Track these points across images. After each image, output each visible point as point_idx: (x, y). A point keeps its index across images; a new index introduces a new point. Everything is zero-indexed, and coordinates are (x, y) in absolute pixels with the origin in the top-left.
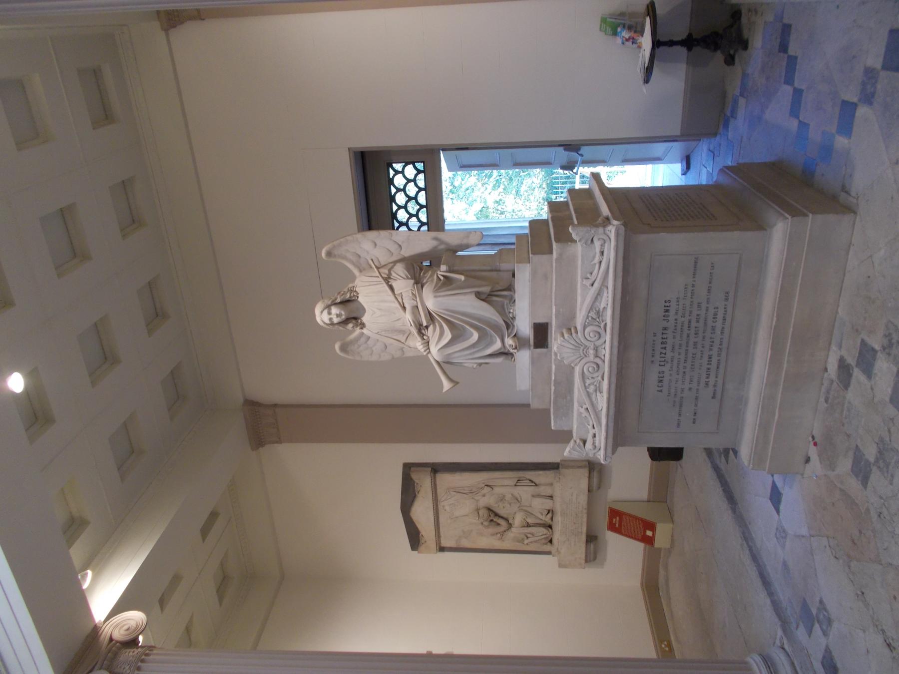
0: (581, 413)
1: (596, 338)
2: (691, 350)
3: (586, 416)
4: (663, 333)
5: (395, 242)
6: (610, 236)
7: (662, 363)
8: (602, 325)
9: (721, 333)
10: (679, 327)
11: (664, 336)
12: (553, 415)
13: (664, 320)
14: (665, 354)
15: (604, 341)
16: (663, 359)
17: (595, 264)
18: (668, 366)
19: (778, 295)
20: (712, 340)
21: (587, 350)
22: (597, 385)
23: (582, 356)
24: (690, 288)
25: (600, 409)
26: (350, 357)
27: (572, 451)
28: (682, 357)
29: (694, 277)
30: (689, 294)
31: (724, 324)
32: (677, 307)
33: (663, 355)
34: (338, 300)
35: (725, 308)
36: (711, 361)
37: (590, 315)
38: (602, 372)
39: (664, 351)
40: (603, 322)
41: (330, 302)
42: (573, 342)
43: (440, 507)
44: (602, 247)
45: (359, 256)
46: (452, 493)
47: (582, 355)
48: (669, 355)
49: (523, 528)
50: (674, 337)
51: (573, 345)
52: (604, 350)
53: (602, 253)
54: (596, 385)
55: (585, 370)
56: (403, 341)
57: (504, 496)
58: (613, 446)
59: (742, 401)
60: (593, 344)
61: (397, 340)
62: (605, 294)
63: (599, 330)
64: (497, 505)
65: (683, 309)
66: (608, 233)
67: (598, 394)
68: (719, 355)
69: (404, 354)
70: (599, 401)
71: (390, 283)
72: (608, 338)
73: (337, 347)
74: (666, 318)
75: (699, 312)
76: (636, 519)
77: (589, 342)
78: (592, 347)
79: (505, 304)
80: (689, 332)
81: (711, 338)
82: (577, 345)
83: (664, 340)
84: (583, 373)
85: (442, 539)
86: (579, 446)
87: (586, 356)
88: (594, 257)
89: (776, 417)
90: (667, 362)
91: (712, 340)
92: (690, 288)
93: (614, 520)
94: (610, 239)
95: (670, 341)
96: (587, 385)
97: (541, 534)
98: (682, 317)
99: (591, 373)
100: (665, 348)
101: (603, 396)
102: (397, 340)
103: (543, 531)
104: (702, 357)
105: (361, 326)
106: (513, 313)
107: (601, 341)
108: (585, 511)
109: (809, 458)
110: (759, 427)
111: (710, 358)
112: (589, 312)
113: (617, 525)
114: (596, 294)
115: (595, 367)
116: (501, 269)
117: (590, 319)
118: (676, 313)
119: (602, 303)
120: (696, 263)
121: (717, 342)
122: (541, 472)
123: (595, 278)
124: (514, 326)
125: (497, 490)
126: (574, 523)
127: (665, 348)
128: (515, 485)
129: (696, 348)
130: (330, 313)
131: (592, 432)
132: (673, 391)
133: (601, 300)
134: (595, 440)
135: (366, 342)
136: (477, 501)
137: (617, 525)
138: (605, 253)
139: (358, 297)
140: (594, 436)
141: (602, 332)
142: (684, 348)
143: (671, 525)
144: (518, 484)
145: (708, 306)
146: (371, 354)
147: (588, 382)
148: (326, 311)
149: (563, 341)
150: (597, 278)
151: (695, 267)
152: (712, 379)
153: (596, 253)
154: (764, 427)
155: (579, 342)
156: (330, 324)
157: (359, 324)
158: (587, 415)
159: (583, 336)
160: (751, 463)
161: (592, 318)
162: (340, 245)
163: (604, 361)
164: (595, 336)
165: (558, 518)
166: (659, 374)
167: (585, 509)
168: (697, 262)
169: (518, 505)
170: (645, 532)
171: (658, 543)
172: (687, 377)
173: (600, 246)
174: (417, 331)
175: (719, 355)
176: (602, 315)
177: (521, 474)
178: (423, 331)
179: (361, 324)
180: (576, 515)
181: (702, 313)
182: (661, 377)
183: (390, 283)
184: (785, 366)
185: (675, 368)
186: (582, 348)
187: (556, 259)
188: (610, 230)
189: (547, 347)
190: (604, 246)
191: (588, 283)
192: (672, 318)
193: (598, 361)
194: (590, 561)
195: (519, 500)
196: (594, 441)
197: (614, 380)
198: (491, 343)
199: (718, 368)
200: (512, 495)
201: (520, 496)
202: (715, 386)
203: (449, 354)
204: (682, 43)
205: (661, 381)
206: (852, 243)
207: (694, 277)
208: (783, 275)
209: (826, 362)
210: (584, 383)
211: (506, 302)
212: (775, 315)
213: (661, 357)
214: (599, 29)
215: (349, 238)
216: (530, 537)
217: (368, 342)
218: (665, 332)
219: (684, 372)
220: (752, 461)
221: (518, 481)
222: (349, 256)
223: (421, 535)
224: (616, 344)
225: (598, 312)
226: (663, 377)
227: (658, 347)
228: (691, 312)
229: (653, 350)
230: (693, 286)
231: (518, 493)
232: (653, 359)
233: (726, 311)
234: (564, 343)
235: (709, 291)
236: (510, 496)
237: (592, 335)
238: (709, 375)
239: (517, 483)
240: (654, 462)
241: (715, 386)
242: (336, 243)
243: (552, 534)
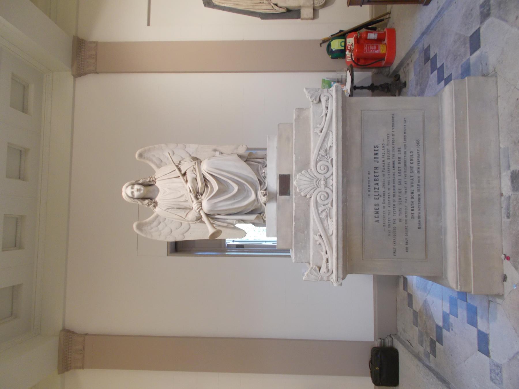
0: (316, 241)
1: (324, 171)
2: (397, 186)
3: (320, 244)
4: (375, 172)
5: (188, 152)
6: (332, 94)
7: (377, 197)
8: (329, 160)
9: (418, 172)
10: (386, 168)
11: (376, 174)
12: (294, 248)
13: (375, 161)
14: (378, 189)
15: (331, 174)
16: (377, 194)
17: (323, 116)
18: (381, 199)
19: (455, 136)
20: (412, 178)
21: (319, 181)
22: (328, 212)
23: (315, 187)
24: (391, 137)
25: (331, 234)
26: (143, 235)
27: (310, 275)
28: (391, 191)
29: (393, 129)
30: (391, 142)
31: (419, 165)
32: (383, 151)
33: (376, 190)
34: (141, 182)
35: (418, 153)
36: (413, 196)
37: (320, 153)
38: (332, 200)
39: (377, 187)
40: (330, 158)
41: (134, 182)
42: (308, 176)
44: (327, 103)
45: (162, 161)
47: (315, 186)
48: (381, 190)
50: (384, 175)
51: (309, 178)
52: (332, 181)
53: (327, 108)
54: (327, 212)
55: (318, 198)
56: (184, 216)
58: (343, 273)
59: (441, 231)
60: (323, 177)
61: (180, 216)
62: (331, 136)
63: (327, 164)
65: (388, 153)
66: (331, 92)
67: (329, 219)
68: (419, 191)
69: (184, 238)
70: (330, 225)
71: (179, 167)
72: (334, 170)
73: (135, 225)
74: (376, 160)
75: (399, 156)
77: (321, 175)
78: (323, 178)
79: (259, 167)
80: (394, 171)
81: (411, 177)
82: (311, 178)
83: (376, 178)
84: (316, 202)
86: (315, 270)
87: (318, 187)
88: (322, 113)
89: (472, 239)
90: (381, 196)
91: (412, 178)
92: (391, 137)
94: (332, 96)
95: (381, 178)
96: (320, 212)
98: (387, 159)
99: (323, 200)
100: (377, 184)
101: (333, 221)
102: (180, 216)
104: (406, 192)
105: (154, 203)
106: (264, 172)
107: (329, 173)
109: (505, 275)
110: (459, 248)
111: (412, 193)
112: (319, 151)
114: (324, 137)
115: (326, 195)
117: (320, 156)
118: (383, 156)
119: (329, 143)
120: (393, 118)
121: (416, 179)
123: (323, 126)
124: (265, 183)
127: (377, 184)
129: (401, 184)
130: (132, 188)
131: (325, 257)
132: (387, 221)
133: (328, 141)
134: (329, 265)
135: (157, 226)
138: (329, 108)
139: (155, 182)
140: (327, 261)
141: (330, 165)
142: (391, 184)
145: (405, 150)
146: (160, 235)
147: (321, 209)
148: (130, 187)
149: (301, 176)
150: (324, 126)
151: (393, 121)
152: (416, 212)
153: (323, 110)
154: (463, 247)
155: (313, 176)
156: (131, 197)
157: (153, 202)
158: (320, 241)
159: (316, 170)
160: (459, 285)
161: (322, 156)
162: (149, 150)
163: (332, 191)
164: (325, 169)
166: (375, 207)
168: (394, 118)
170: (375, 369)
172: (397, 210)
173: (325, 102)
174: (194, 195)
175: (419, 191)
176: (329, 153)
178: (199, 197)
179: (154, 202)
181: (402, 156)
182: (377, 209)
183: (179, 167)
184: (470, 192)
185: (387, 201)
186: (315, 180)
187: (295, 119)
188: (332, 277)
189: (289, 195)
190: (328, 102)
191: (318, 131)
192: (380, 159)
193: (329, 191)
196: (327, 265)
197: (341, 205)
198: (247, 197)
199: (419, 201)
202: (419, 217)
203: (215, 203)
204: (368, 88)
205: (377, 213)
206: (499, 95)
207: (393, 129)
208: (455, 121)
209: (500, 188)
210: (318, 210)
211: (260, 165)
212: (455, 151)
213: (375, 192)
214: (320, 43)
215: (156, 146)
217: (159, 227)
218: (376, 171)
219: (394, 205)
220: (459, 283)
222: (154, 159)
224: (340, 173)
225: (326, 150)
226: (378, 209)
227: (372, 183)
228: (394, 155)
229: (369, 186)
230: (393, 135)
232: (369, 193)
233: (419, 155)
234: (301, 177)
235: (405, 139)
237: (322, 168)
238: (413, 207)
240: (377, 387)
241: (419, 217)
242: (147, 148)
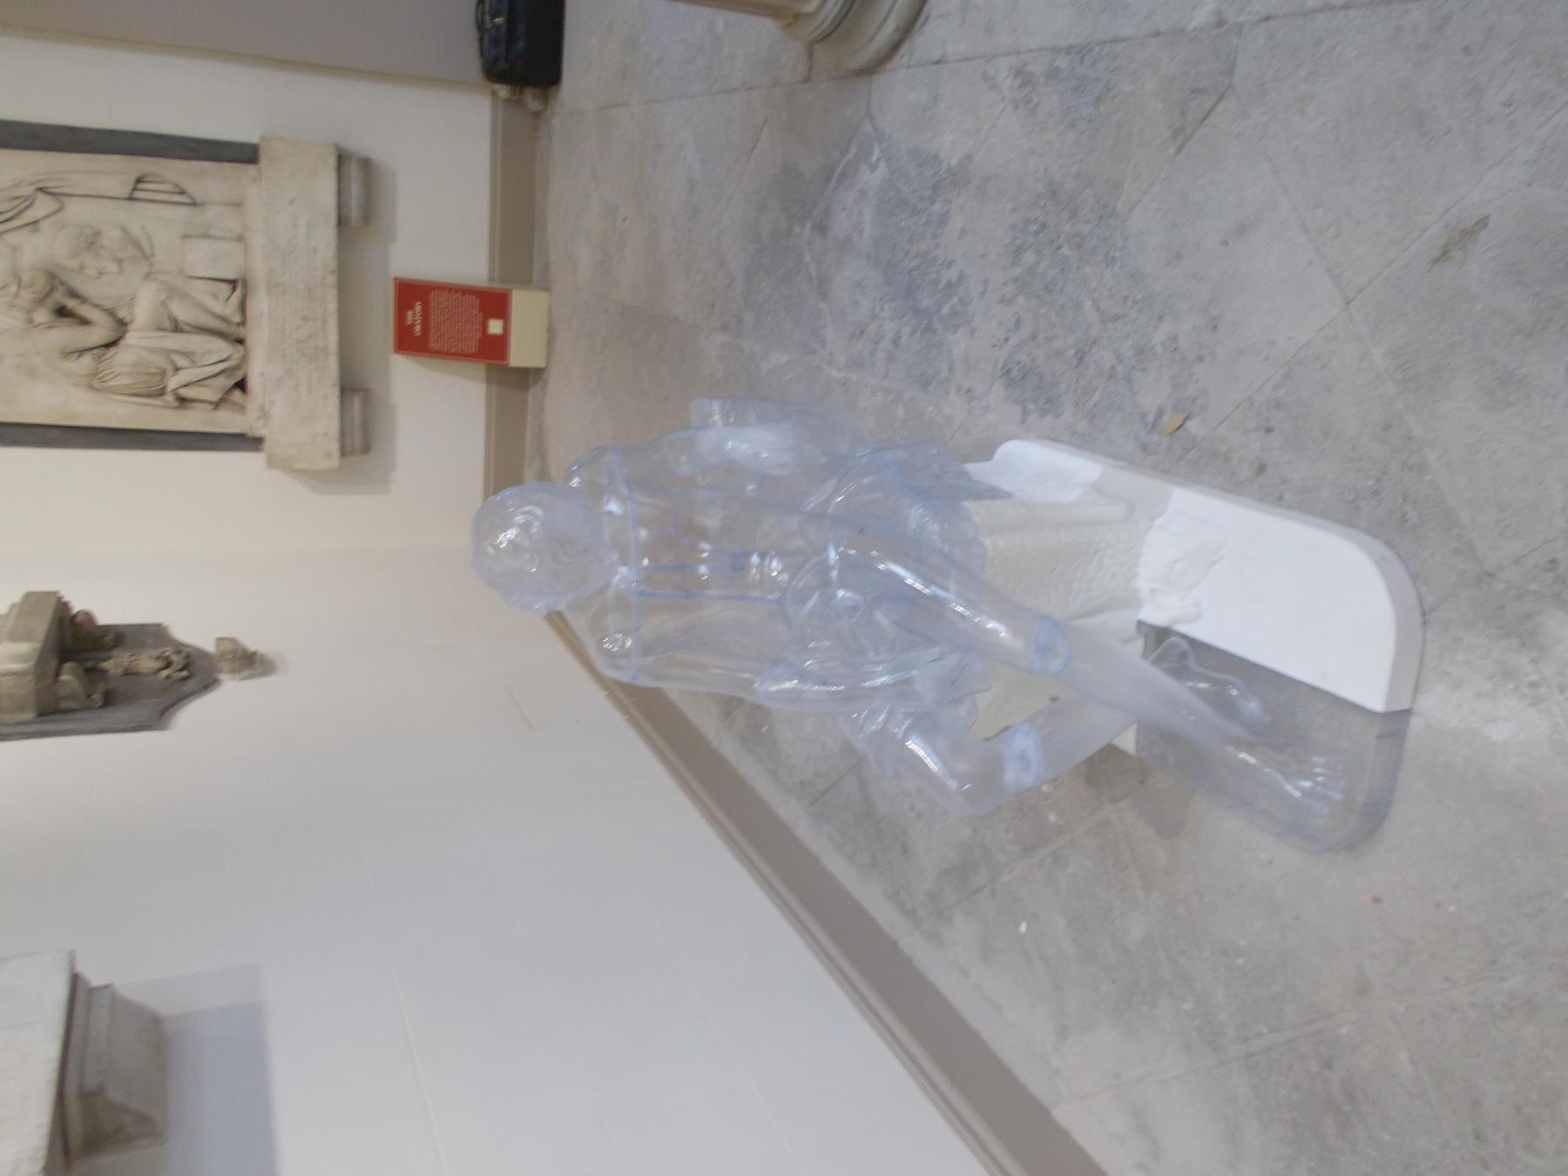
49: (160, 334)
57: (97, 234)
103: (222, 348)
116: (141, 670)
128: (131, 199)
136: (15, 249)
137: (418, 328)
143: (544, 296)
144: (138, 194)
165: (260, 304)
167: (332, 272)
169: (144, 268)
170: (485, 326)
171: (520, 355)
177: (145, 165)
194: (353, 453)
200: (124, 230)
201: (149, 238)
236: (117, 233)
239: (135, 189)
243: (245, 359)
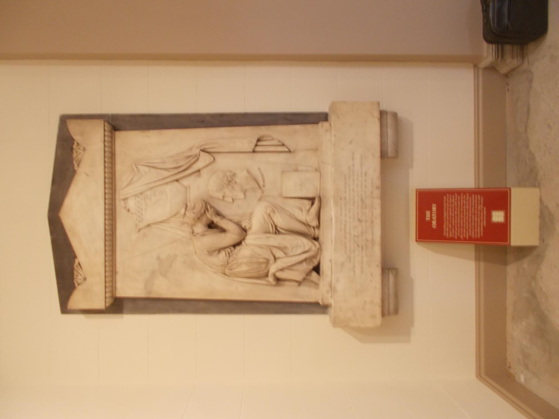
43: (120, 205)
46: (141, 168)
64: (220, 195)
76: (459, 239)
85: (119, 278)
93: (428, 213)
97: (299, 251)
108: (377, 193)
113: (434, 223)
122: (298, 127)
125: (223, 162)
126: (360, 221)
128: (254, 152)
136: (187, 188)
137: (434, 223)
144: (258, 149)
167: (377, 188)
170: (489, 216)
177: (263, 131)
180: (362, 200)
181: (450, 206)
195: (261, 183)
200: (248, 171)
201: (262, 175)
216: (279, 258)
221: (259, 140)
223: (76, 263)
231: (259, 169)
236: (245, 173)
239: (256, 145)
243: (320, 250)
